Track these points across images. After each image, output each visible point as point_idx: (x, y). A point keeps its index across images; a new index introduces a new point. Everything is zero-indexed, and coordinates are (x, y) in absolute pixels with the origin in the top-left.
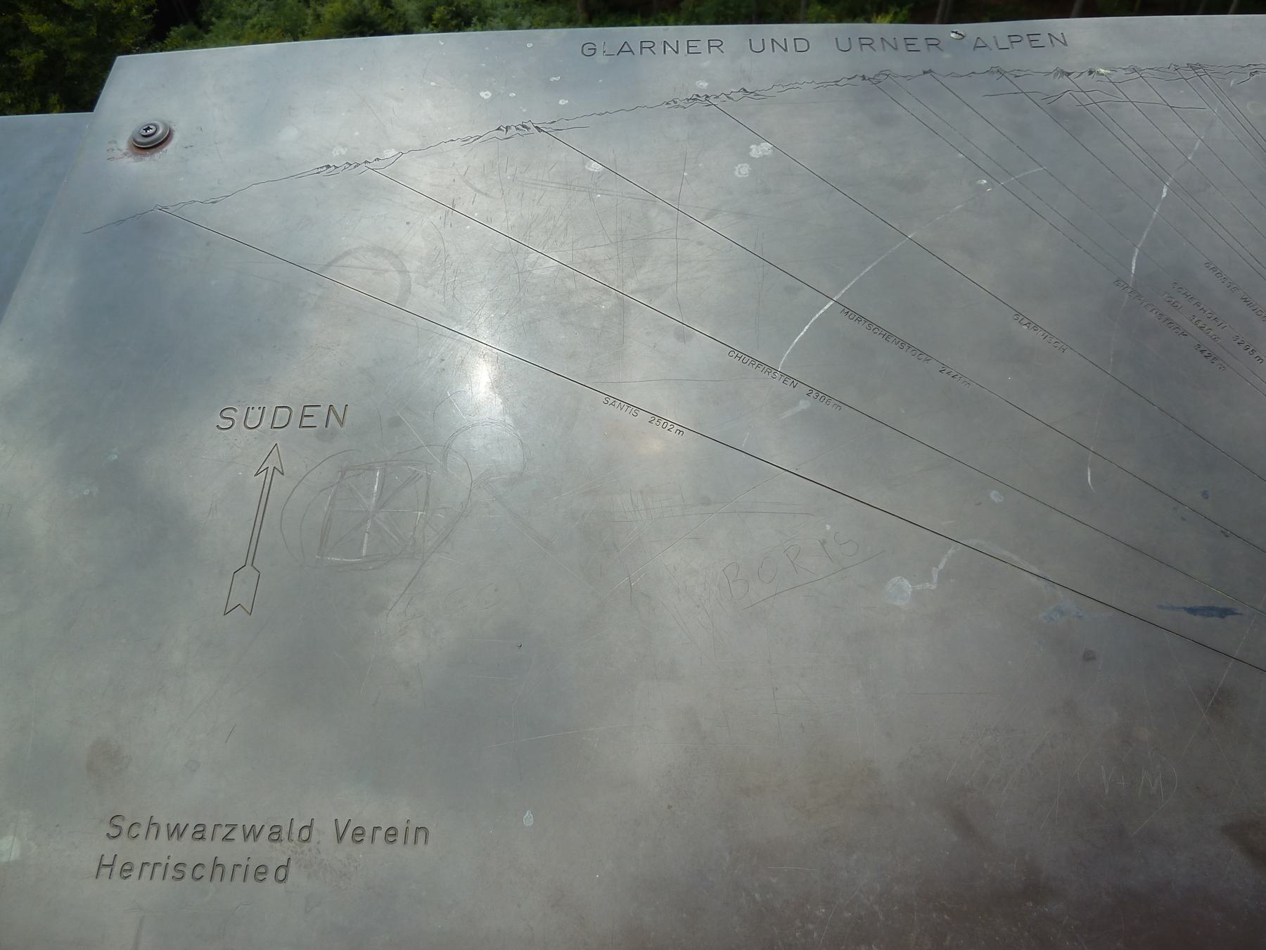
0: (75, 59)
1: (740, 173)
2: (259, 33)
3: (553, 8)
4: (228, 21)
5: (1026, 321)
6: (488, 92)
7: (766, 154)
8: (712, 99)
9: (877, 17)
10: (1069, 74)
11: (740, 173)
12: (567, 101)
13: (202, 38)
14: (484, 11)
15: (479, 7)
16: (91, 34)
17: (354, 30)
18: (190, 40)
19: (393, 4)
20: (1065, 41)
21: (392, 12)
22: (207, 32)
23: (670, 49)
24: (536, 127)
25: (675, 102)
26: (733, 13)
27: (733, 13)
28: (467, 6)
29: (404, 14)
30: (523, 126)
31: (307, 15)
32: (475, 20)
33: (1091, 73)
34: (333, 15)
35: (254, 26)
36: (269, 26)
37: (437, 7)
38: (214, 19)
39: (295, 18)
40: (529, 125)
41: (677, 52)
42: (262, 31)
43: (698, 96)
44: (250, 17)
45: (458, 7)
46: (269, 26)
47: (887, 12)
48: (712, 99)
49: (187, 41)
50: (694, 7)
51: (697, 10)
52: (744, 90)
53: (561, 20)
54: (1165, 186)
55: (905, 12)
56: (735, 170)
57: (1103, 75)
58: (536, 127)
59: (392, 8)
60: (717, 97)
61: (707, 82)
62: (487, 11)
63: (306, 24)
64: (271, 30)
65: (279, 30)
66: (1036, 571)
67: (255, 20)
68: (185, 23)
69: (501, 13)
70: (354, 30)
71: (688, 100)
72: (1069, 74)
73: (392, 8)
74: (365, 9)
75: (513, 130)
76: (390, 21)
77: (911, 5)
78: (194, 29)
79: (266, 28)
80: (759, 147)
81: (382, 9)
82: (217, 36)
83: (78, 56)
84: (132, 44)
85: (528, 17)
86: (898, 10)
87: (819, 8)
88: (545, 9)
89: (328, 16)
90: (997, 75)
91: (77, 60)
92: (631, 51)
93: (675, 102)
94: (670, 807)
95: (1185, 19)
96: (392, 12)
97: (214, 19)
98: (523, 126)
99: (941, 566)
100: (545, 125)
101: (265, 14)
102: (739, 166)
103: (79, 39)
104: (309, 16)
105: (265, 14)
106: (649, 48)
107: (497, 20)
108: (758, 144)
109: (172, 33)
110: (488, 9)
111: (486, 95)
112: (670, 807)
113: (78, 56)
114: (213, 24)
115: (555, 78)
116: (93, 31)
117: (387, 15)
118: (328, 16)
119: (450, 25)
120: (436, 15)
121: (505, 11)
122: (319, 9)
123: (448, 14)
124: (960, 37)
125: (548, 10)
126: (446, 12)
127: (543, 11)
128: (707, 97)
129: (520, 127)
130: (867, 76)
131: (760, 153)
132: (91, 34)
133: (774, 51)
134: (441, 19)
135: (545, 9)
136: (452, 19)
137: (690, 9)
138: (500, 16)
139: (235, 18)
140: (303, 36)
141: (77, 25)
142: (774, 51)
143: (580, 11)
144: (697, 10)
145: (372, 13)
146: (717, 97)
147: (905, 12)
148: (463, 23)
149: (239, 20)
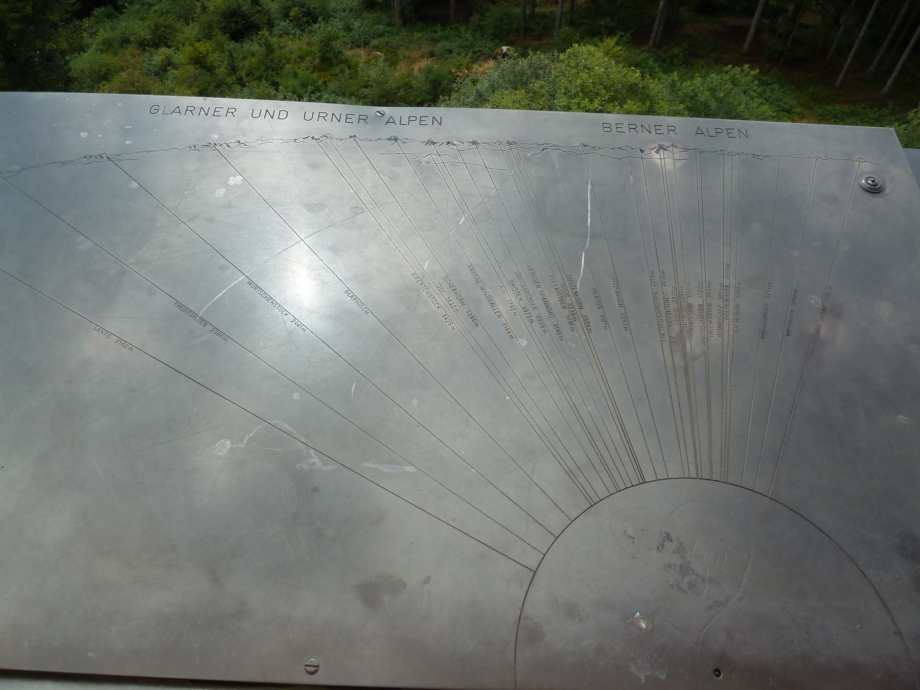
0: (14, 28)
1: (218, 194)
2: (159, 17)
3: (379, 14)
4: (137, 6)
5: (352, 294)
6: (86, 133)
7: (238, 183)
8: (217, 147)
9: (607, 38)
10: (435, 143)
11: (218, 194)
12: (131, 142)
13: (117, 17)
14: (327, 13)
15: (324, 10)
16: (27, 11)
17: (230, 20)
18: (108, 18)
19: (261, 3)
20: (441, 122)
21: (260, 8)
22: (121, 13)
23: (203, 112)
24: (108, 157)
25: (195, 147)
26: (506, 27)
27: (506, 27)
28: (315, 8)
29: (268, 11)
30: (100, 156)
31: (197, 6)
32: (320, 18)
33: (448, 143)
34: (216, 8)
35: (156, 12)
36: (168, 12)
37: (293, 7)
38: (127, 4)
39: (187, 8)
40: (104, 156)
41: (206, 115)
42: (162, 16)
43: (210, 143)
44: (153, 5)
45: (308, 9)
46: (168, 12)
47: (616, 35)
48: (217, 147)
49: (105, 19)
50: (480, 21)
51: (481, 23)
52: (239, 141)
53: (383, 23)
54: (464, 217)
55: (628, 35)
56: (216, 192)
57: (455, 145)
58: (108, 157)
59: (259, 5)
60: (221, 145)
61: (219, 135)
62: (330, 13)
63: (195, 13)
64: (169, 15)
65: (175, 16)
66: (303, 440)
67: (157, 7)
68: (105, 5)
69: (340, 15)
70: (230, 20)
71: (203, 146)
72: (435, 143)
73: (259, 5)
74: (239, 4)
75: (93, 159)
76: (257, 15)
77: (633, 31)
78: (112, 10)
79: (166, 13)
80: (235, 179)
81: (252, 6)
82: (128, 17)
83: (16, 27)
84: (59, 20)
85: (359, 20)
86: (623, 34)
87: (568, 28)
88: (372, 14)
89: (212, 8)
90: (393, 142)
91: (15, 30)
92: (180, 112)
93: (195, 147)
94: (57, 560)
95: (518, 112)
96: (260, 8)
97: (127, 4)
98: (100, 156)
99: (251, 435)
100: (113, 157)
101: (165, 3)
102: (219, 189)
103: (18, 15)
104: (198, 7)
105: (165, 3)
106: (173, 112)
107: (337, 20)
108: (235, 176)
109: (95, 12)
110: (331, 11)
111: (84, 135)
112: (57, 560)
113: (16, 27)
114: (126, 8)
115: (128, 127)
116: (29, 9)
117: (256, 11)
118: (212, 8)
119: (301, 21)
120: (292, 14)
121: (343, 14)
122: (206, 2)
123: (301, 13)
124: (381, 115)
125: (374, 15)
126: (299, 11)
127: (370, 16)
128: (215, 144)
129: (98, 157)
130: (316, 137)
131: (234, 182)
132: (27, 11)
133: (265, 118)
134: (295, 17)
135: (372, 14)
136: (303, 17)
137: (476, 22)
138: (339, 17)
139: (143, 4)
140: (193, 21)
141: (17, 4)
142: (265, 118)
143: (397, 18)
144: (481, 23)
145: (245, 8)
146: (221, 145)
147: (628, 35)
148: (311, 21)
149: (145, 6)
